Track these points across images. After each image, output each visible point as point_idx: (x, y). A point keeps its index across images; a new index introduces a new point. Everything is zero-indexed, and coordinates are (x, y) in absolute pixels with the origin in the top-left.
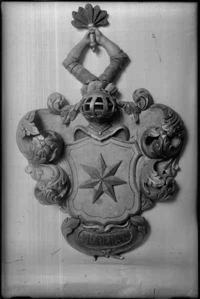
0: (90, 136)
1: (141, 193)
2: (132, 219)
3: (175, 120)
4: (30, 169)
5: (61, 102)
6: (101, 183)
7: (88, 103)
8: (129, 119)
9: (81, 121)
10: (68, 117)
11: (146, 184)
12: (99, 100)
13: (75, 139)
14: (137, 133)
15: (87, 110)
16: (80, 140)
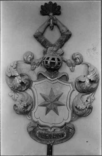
0: (47, 77)
1: (73, 111)
2: (67, 125)
3: (94, 73)
4: (11, 94)
5: (31, 57)
6: (51, 105)
7: (47, 60)
8: (65, 69)
9: (39, 69)
10: (35, 66)
11: (76, 107)
12: (53, 59)
13: (38, 78)
14: (73, 77)
15: (46, 64)
16: (41, 79)
